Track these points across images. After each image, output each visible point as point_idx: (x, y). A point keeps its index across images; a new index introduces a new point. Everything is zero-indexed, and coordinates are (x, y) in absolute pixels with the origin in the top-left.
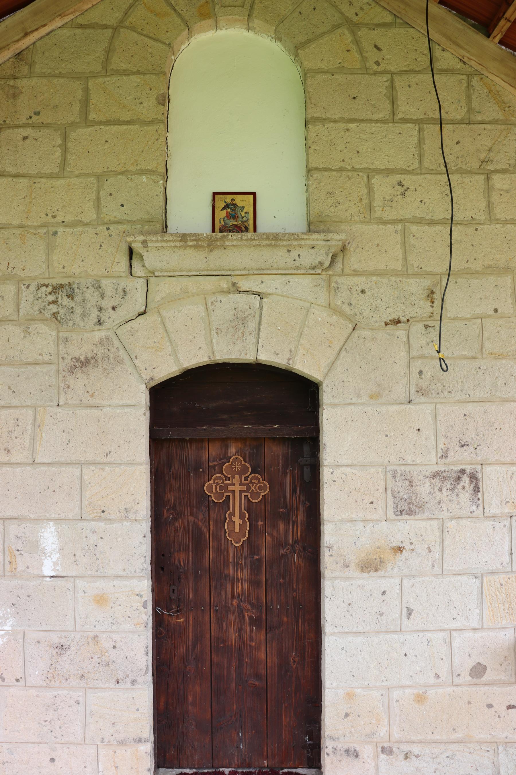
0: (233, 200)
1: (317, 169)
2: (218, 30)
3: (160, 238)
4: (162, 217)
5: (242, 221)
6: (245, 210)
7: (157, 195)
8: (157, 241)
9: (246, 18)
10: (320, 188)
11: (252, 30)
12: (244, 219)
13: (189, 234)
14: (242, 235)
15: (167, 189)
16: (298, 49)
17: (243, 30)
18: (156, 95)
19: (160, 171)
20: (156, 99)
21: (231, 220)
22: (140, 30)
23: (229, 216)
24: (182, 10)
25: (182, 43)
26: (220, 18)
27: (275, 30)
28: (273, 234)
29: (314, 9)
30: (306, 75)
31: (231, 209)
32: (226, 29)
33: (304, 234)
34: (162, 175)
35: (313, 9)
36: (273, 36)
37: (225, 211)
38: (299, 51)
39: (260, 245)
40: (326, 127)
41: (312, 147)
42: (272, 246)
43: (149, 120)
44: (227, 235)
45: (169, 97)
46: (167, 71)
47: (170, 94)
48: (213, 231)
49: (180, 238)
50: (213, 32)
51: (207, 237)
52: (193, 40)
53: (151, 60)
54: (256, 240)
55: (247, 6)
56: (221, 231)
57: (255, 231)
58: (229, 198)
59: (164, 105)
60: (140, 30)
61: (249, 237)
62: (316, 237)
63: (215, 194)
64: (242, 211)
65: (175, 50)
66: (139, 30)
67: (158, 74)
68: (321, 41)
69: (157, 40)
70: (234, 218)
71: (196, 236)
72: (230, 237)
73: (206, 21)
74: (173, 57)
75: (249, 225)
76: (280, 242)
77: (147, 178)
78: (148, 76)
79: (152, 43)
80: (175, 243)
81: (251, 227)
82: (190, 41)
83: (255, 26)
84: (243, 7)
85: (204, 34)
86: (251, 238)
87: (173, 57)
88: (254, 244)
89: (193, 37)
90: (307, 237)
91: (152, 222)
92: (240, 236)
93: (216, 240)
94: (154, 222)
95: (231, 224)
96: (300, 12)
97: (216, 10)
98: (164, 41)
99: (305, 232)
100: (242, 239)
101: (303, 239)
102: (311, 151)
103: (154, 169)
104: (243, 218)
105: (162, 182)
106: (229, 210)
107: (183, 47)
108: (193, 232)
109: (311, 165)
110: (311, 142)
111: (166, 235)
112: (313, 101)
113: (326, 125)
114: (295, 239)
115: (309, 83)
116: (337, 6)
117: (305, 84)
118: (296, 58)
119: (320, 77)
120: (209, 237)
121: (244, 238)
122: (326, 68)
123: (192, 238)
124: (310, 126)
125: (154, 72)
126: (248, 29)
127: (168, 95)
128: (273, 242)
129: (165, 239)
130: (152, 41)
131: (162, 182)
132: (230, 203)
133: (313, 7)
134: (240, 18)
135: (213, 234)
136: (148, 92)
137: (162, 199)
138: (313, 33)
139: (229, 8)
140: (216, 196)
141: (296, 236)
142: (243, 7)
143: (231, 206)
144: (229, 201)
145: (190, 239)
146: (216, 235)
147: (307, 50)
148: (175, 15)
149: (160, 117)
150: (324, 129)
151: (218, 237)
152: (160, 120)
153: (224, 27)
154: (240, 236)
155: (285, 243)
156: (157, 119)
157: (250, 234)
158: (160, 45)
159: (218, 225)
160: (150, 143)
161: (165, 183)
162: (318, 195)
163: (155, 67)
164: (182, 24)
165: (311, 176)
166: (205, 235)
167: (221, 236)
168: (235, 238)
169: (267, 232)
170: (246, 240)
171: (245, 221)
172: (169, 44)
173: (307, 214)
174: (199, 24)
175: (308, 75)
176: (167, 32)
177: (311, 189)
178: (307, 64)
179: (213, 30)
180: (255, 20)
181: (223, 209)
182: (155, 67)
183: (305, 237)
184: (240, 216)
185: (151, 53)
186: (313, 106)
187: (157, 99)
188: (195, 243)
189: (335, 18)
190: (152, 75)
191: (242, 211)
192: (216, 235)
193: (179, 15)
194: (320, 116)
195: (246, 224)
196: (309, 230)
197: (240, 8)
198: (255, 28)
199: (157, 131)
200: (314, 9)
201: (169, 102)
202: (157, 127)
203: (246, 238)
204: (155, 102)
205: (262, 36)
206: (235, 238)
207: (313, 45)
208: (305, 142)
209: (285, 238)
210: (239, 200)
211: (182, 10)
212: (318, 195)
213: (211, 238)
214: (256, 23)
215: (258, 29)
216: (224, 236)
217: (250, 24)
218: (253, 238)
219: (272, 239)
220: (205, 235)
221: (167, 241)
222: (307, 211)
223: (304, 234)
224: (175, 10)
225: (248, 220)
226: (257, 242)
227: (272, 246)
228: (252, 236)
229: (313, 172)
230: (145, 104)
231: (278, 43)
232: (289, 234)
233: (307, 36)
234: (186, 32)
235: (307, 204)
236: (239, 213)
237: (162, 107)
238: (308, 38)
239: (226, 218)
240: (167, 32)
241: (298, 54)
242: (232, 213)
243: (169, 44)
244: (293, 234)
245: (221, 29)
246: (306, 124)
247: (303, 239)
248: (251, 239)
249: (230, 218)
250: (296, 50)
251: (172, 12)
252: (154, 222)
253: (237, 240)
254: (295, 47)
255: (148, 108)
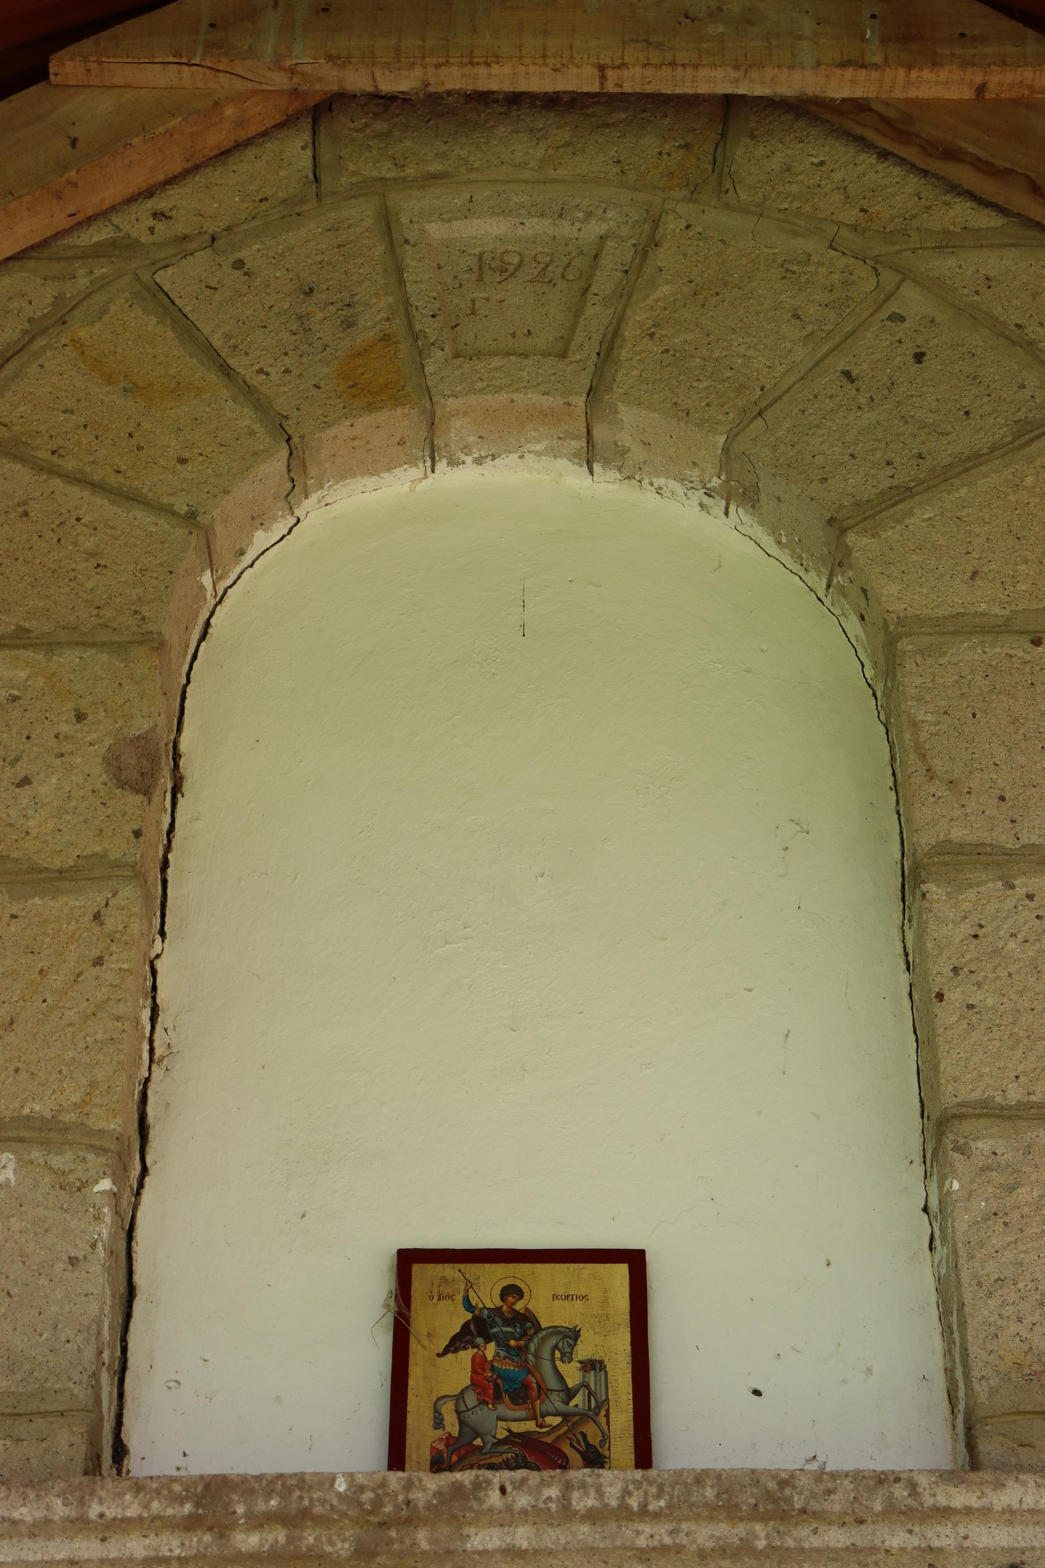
0: (512, 1291)
1: (988, 1111)
2: (441, 466)
3: (60, 1510)
4: (96, 1388)
5: (566, 1416)
6: (584, 1351)
7: (73, 1261)
8: (42, 1529)
9: (579, 401)
10: (1015, 1216)
11: (606, 463)
12: (578, 1400)
13: (244, 1479)
14: (568, 1487)
15: (140, 1233)
16: (843, 531)
17: (563, 463)
18: (108, 742)
19: (102, 1125)
20: (106, 760)
21: (502, 1409)
22: (47, 455)
23: (488, 1386)
24: (260, 371)
25: (259, 520)
26: (452, 403)
27: (726, 450)
28: (755, 1476)
29: (919, 357)
30: (890, 650)
31: (502, 1343)
32: (479, 461)
33: (947, 1477)
34: (114, 1147)
35: (910, 358)
36: (715, 482)
37: (466, 1356)
38: (851, 538)
39: (679, 1549)
40: (1020, 891)
41: (955, 996)
42: (756, 1554)
43: (57, 864)
44: (477, 1486)
45: (176, 766)
46: (172, 637)
47: (183, 747)
48: (397, 1459)
49: (188, 1508)
50: (415, 473)
51: (352, 1498)
52: (310, 508)
53: (89, 585)
54: (657, 1516)
55: (586, 349)
56: (438, 1465)
57: (644, 1457)
58: (488, 1282)
59: (147, 793)
60: (47, 455)
61: (612, 1494)
62: (1029, 1502)
63: (408, 1260)
64: (567, 1357)
65: (221, 544)
66: (43, 454)
67: (120, 648)
68: (963, 492)
69: (131, 498)
70: (522, 1393)
71: (286, 1492)
72: (494, 1497)
73: (382, 416)
74: (207, 579)
75: (605, 1438)
76: (803, 1531)
77: (23, 1163)
78: (70, 657)
79: (101, 507)
80: (152, 1540)
81: (622, 1446)
82: (299, 512)
83: (625, 439)
84: (563, 356)
85: (370, 482)
86: (623, 1506)
87: (207, 579)
88: (642, 1542)
89: (314, 497)
90: (974, 1502)
91: (30, 1417)
92: (553, 1492)
93: (410, 1518)
94: (44, 1414)
95: (502, 1434)
96: (847, 374)
97: (428, 370)
98: (166, 500)
99: (946, 1465)
100: (567, 1513)
101: (945, 1513)
102: (947, 1015)
103: (70, 1117)
104: (570, 1394)
105: (105, 1184)
106: (491, 1350)
107: (261, 539)
108: (270, 1468)
109: (959, 1087)
110: (947, 970)
111: (108, 1486)
112: (939, 765)
113: (1023, 884)
114: (893, 1513)
115: (912, 678)
116: (1031, 343)
117: (887, 692)
118: (839, 579)
119: (967, 653)
120: (367, 1496)
121: (582, 1502)
122: (997, 610)
123: (261, 1506)
124: (930, 887)
125: (107, 637)
126: (590, 457)
127: (177, 756)
128: (758, 1527)
129: (94, 1510)
130: (101, 501)
131: (105, 1184)
132: (498, 1310)
133: (909, 349)
134: (546, 402)
135: (395, 1478)
136: (65, 728)
137: (97, 1283)
138: (920, 456)
139: (496, 362)
140: (416, 1268)
141: (900, 1492)
142: (563, 356)
143: (505, 1333)
144: (488, 1298)
145: (249, 1515)
146: (409, 1485)
147: (891, 534)
148: (226, 393)
149: (120, 847)
150: (1010, 903)
151: (419, 1497)
152: (117, 865)
153: (466, 449)
154: (553, 1492)
155: (836, 1537)
156: (103, 856)
157: (614, 1482)
158: (142, 516)
159: (421, 1436)
160: (57, 980)
161: (127, 1199)
162: (1008, 1256)
163: (108, 613)
164: (258, 428)
165: (957, 1149)
166: (341, 1486)
167: (438, 1494)
168: (523, 1501)
169: (718, 1466)
170: (592, 1516)
171: (585, 1417)
172: (191, 516)
173: (949, 1371)
174: (342, 430)
175: (905, 645)
176: (182, 461)
177: (962, 1221)
178: (893, 596)
179: (413, 462)
180: (622, 408)
181: (456, 1344)
182: (108, 613)
183: (960, 1498)
184: (552, 1383)
185: (92, 554)
186: (943, 791)
187: (113, 762)
188: (279, 1535)
189: (1027, 393)
190: (89, 653)
191: (567, 1357)
192: (409, 1485)
193: (248, 393)
194: (986, 837)
195: (590, 1430)
196: (972, 1460)
197: (550, 361)
198: (623, 452)
199: (97, 916)
200: (919, 357)
201: (176, 790)
202: (100, 900)
203: (591, 1502)
204: (100, 775)
205: (659, 491)
206: (523, 1501)
207: (922, 514)
208: (904, 978)
209: (836, 1504)
210: (546, 1295)
211: (260, 371)
212: (1008, 1256)
213: (378, 1503)
214: (629, 422)
215: (638, 454)
216: (458, 1490)
217: (600, 433)
218: (634, 1502)
219: (756, 1514)
220: (341, 1486)
221: (109, 1528)
222: (948, 1352)
223: (947, 1477)
224: (226, 370)
225: (600, 1406)
226: (661, 1533)
227: (756, 1554)
228: (626, 1492)
229: (967, 1127)
230: (46, 789)
231: (739, 514)
232: (857, 1477)
233: (889, 470)
234: (276, 465)
235: (944, 1315)
236: (546, 1367)
237: (140, 798)
238: (895, 482)
239: (471, 1399)
240: (182, 461)
241: (848, 551)
242: (508, 1367)
243: (191, 516)
244: (881, 1479)
245: (453, 463)
246: (911, 883)
247: (945, 1513)
248: (623, 1513)
249: (497, 1398)
250: (832, 544)
251: (213, 377)
252: (44, 1414)
253: (537, 1515)
254: (831, 521)
255: (61, 806)
